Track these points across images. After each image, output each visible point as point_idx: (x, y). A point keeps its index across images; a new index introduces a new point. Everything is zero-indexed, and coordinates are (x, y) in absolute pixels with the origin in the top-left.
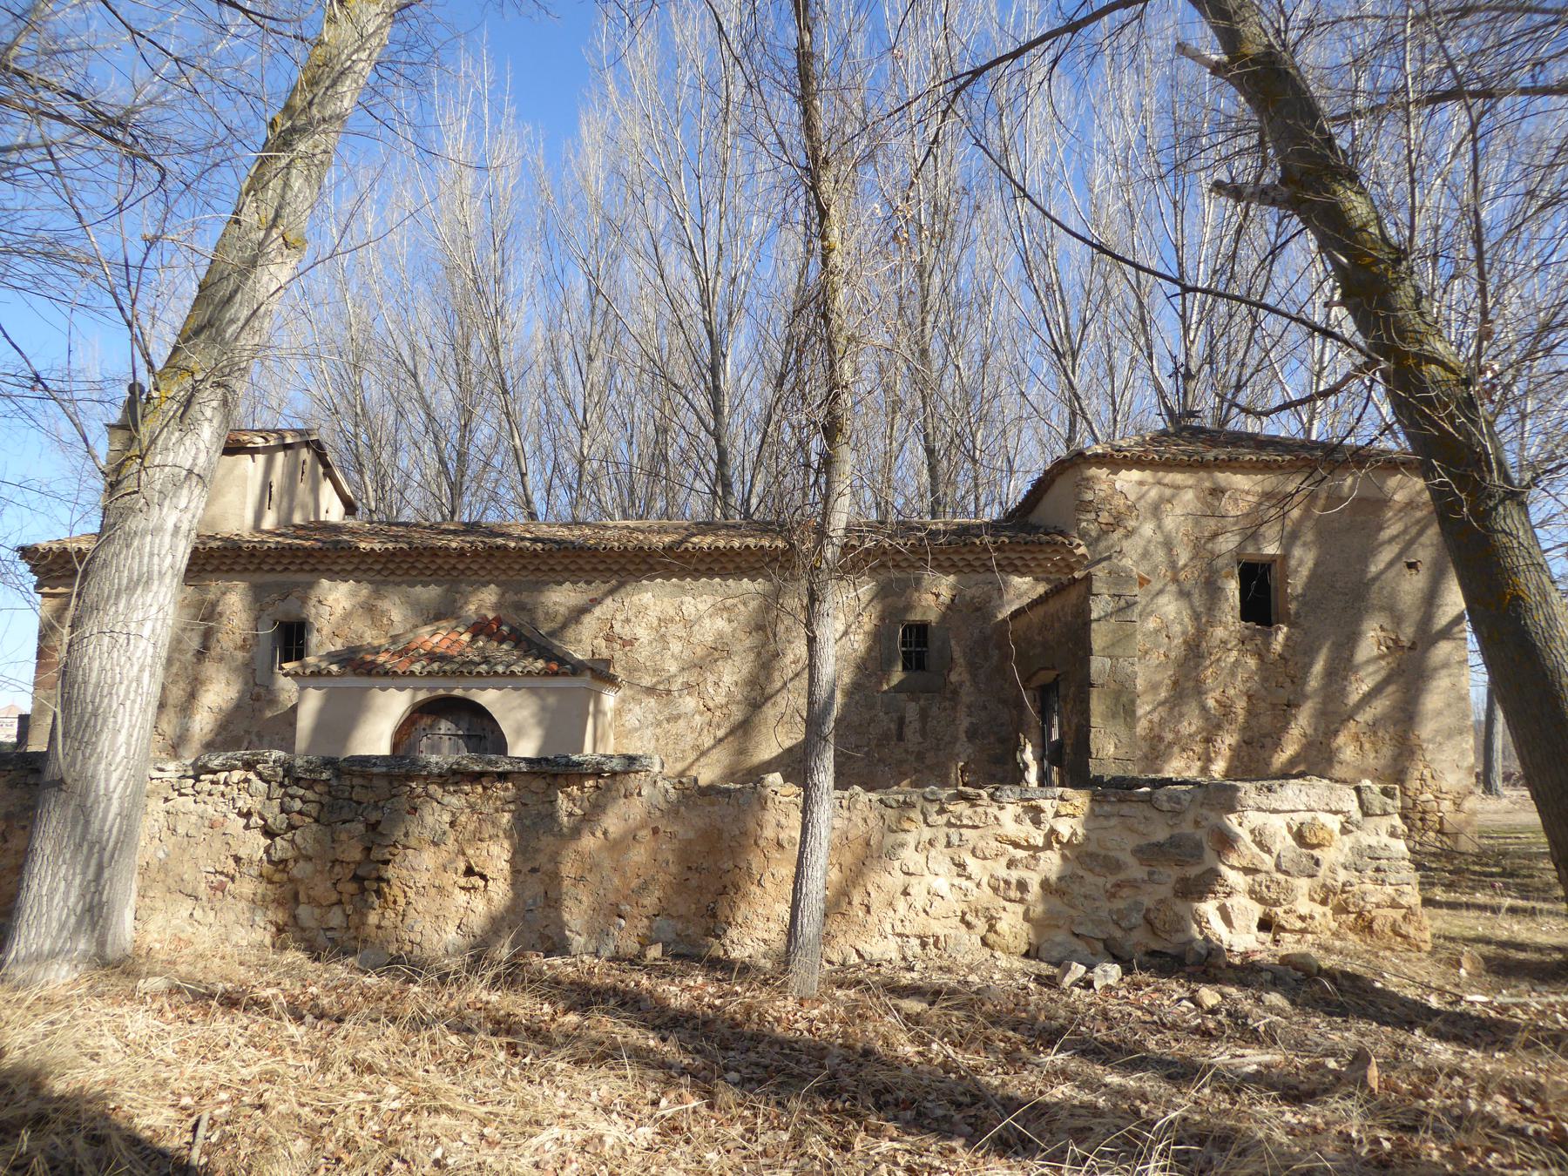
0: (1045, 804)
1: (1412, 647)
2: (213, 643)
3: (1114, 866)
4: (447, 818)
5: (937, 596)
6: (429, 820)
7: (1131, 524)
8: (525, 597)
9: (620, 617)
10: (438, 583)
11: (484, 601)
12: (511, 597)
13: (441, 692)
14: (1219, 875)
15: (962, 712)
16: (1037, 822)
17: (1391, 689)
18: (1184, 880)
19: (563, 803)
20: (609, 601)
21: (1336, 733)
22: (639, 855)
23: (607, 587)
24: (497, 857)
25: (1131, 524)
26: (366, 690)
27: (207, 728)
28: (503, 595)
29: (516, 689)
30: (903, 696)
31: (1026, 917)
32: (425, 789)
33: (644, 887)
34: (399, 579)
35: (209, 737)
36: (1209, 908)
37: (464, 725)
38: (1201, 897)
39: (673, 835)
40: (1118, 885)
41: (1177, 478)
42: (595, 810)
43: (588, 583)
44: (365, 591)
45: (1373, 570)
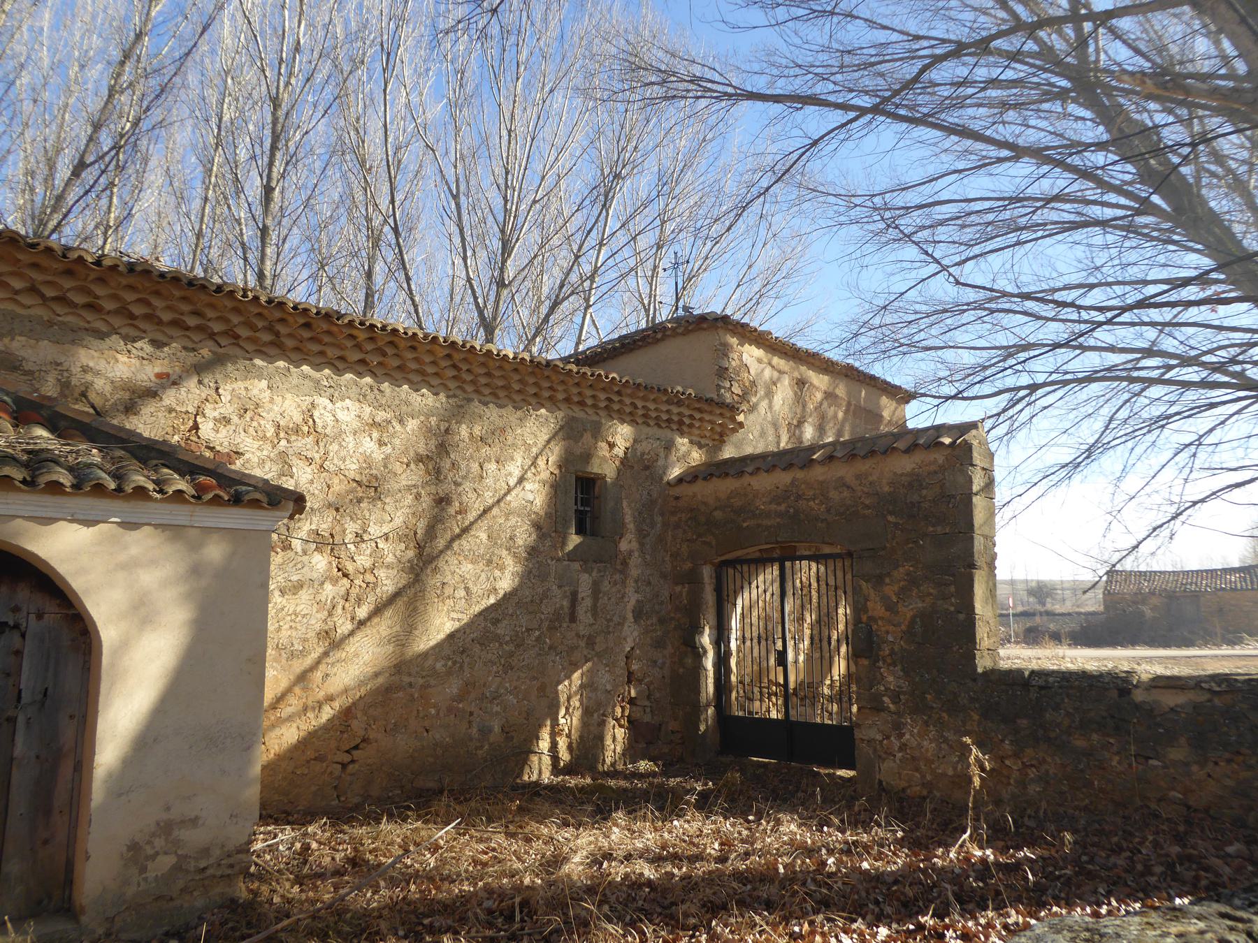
7: (754, 400)
15: (630, 583)
20: (192, 383)
23: (191, 358)
29: (128, 525)
30: (576, 566)
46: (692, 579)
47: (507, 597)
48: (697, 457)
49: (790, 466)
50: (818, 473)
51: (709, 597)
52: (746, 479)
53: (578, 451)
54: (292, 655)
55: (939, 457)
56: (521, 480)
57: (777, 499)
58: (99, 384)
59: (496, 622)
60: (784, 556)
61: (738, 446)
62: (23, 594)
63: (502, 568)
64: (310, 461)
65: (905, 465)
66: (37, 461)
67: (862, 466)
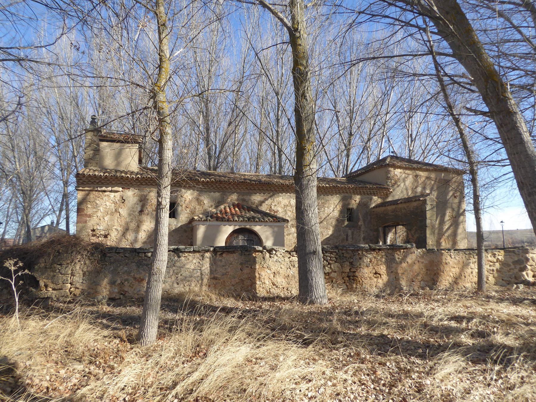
0: (496, 253)
1: (455, 218)
2: (145, 209)
3: (509, 265)
4: (369, 260)
5: (355, 201)
6: (365, 261)
7: (399, 183)
8: (245, 197)
9: (273, 204)
10: (218, 192)
11: (233, 198)
12: (241, 197)
13: (243, 227)
14: (526, 267)
15: (362, 232)
16: (495, 257)
17: (452, 227)
18: (520, 268)
19: (397, 256)
20: (270, 199)
21: (441, 239)
22: (416, 267)
23: (269, 195)
24: (383, 269)
25: (399, 183)
26: (219, 226)
27: (143, 237)
28: (238, 196)
29: (265, 226)
30: (347, 228)
31: (494, 277)
32: (362, 253)
33: (418, 275)
34: (206, 190)
35: (145, 240)
36: (524, 273)
37: (247, 236)
38: (523, 271)
39: (422, 263)
40: (510, 269)
41: (408, 172)
42: (405, 257)
43: (264, 194)
44: (196, 193)
45: (448, 197)
46: (377, 231)
47: (331, 235)
48: (379, 201)
49: (394, 204)
50: (400, 206)
51: (381, 234)
52: (387, 207)
53: (347, 203)
54: (289, 247)
55: (421, 202)
56: (333, 210)
57: (392, 212)
58: (256, 201)
59: (329, 241)
60: (395, 225)
61: (393, 196)
62: (253, 236)
63: (330, 229)
64: (290, 211)
65: (415, 204)
66: (254, 218)
67: (408, 204)
